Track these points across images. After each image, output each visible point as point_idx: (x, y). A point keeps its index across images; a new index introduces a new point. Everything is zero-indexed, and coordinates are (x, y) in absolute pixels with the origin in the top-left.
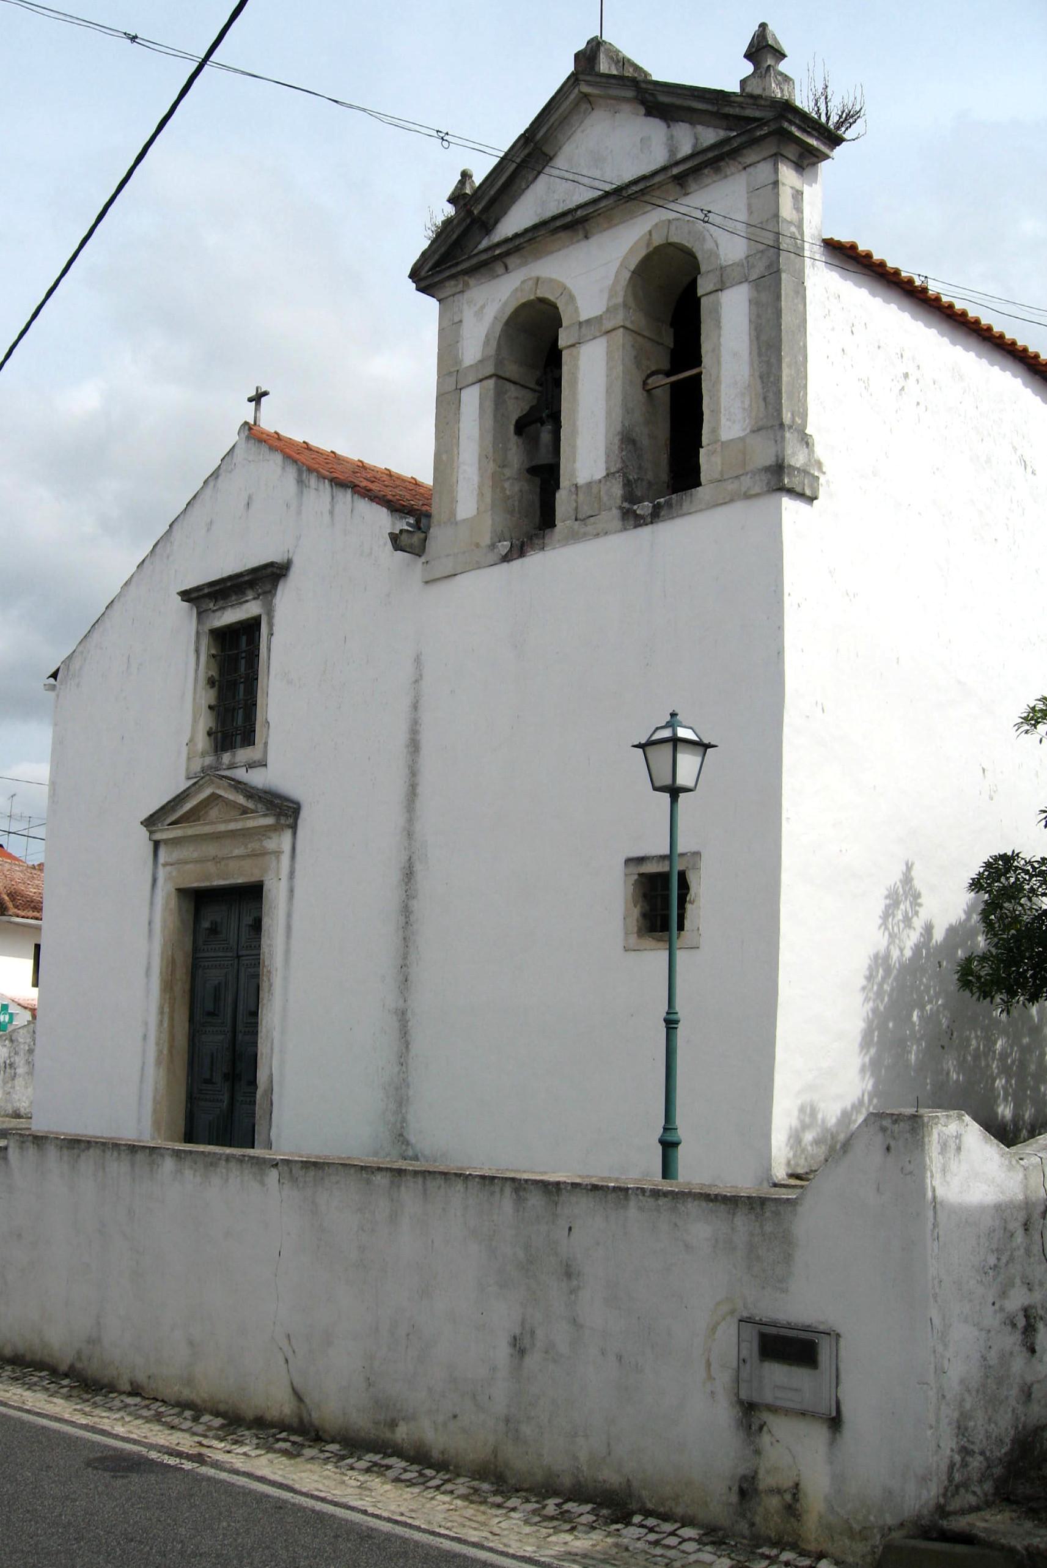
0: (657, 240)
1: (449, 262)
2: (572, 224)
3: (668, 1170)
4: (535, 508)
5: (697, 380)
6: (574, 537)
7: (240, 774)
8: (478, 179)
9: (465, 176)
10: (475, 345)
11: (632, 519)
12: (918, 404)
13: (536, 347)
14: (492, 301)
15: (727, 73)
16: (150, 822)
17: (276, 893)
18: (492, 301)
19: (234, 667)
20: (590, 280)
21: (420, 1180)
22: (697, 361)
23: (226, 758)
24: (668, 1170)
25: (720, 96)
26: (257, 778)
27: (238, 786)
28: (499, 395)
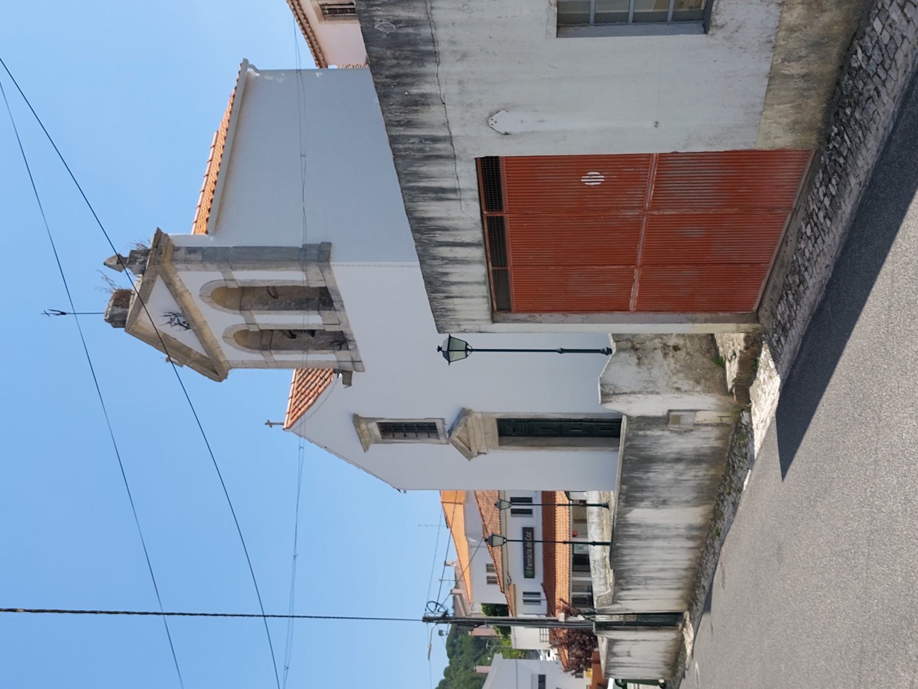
1: (214, 369)
14: (230, 352)
16: (469, 457)
17: (498, 416)
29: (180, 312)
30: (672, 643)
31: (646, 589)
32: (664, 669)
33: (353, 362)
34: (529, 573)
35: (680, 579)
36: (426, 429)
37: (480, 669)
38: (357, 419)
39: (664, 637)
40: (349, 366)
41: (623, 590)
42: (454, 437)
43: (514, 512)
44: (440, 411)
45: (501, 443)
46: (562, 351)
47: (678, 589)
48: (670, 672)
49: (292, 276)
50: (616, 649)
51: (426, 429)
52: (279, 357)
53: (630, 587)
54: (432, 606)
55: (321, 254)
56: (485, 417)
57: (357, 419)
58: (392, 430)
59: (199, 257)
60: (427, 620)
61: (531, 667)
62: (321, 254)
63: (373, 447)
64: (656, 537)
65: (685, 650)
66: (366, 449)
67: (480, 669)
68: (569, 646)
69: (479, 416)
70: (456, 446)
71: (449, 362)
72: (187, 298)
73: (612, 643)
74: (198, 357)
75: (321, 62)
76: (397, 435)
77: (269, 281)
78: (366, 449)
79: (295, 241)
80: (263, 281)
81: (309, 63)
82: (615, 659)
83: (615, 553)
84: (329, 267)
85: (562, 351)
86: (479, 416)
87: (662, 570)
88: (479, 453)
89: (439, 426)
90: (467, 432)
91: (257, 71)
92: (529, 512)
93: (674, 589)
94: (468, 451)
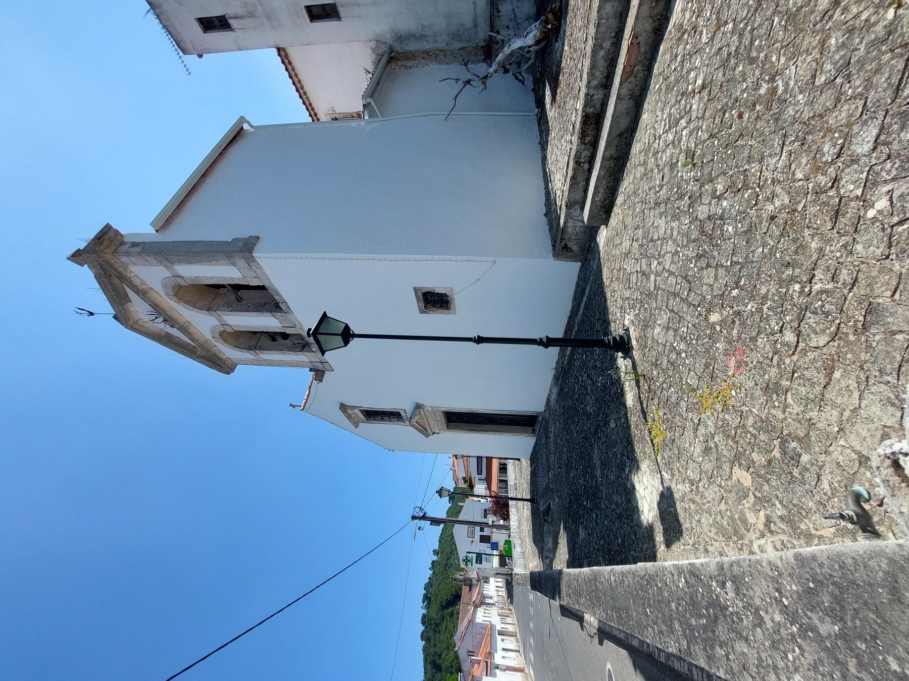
0: (175, 299)
1: (225, 367)
2: (184, 329)
11: (289, 311)
14: (228, 352)
16: (427, 436)
17: (443, 409)
18: (228, 352)
20: (204, 323)
34: (479, 472)
36: (393, 416)
37: (460, 504)
40: (320, 366)
42: (414, 422)
44: (404, 405)
45: (448, 428)
46: (480, 340)
49: (225, 272)
51: (393, 416)
52: (266, 356)
55: (245, 248)
56: (434, 411)
57: (343, 407)
58: (372, 415)
59: (138, 249)
62: (245, 248)
63: (361, 425)
67: (460, 504)
70: (416, 428)
72: (153, 295)
76: (377, 418)
77: (212, 278)
79: (226, 235)
80: (206, 278)
85: (480, 340)
86: (430, 409)
88: (434, 433)
89: (403, 414)
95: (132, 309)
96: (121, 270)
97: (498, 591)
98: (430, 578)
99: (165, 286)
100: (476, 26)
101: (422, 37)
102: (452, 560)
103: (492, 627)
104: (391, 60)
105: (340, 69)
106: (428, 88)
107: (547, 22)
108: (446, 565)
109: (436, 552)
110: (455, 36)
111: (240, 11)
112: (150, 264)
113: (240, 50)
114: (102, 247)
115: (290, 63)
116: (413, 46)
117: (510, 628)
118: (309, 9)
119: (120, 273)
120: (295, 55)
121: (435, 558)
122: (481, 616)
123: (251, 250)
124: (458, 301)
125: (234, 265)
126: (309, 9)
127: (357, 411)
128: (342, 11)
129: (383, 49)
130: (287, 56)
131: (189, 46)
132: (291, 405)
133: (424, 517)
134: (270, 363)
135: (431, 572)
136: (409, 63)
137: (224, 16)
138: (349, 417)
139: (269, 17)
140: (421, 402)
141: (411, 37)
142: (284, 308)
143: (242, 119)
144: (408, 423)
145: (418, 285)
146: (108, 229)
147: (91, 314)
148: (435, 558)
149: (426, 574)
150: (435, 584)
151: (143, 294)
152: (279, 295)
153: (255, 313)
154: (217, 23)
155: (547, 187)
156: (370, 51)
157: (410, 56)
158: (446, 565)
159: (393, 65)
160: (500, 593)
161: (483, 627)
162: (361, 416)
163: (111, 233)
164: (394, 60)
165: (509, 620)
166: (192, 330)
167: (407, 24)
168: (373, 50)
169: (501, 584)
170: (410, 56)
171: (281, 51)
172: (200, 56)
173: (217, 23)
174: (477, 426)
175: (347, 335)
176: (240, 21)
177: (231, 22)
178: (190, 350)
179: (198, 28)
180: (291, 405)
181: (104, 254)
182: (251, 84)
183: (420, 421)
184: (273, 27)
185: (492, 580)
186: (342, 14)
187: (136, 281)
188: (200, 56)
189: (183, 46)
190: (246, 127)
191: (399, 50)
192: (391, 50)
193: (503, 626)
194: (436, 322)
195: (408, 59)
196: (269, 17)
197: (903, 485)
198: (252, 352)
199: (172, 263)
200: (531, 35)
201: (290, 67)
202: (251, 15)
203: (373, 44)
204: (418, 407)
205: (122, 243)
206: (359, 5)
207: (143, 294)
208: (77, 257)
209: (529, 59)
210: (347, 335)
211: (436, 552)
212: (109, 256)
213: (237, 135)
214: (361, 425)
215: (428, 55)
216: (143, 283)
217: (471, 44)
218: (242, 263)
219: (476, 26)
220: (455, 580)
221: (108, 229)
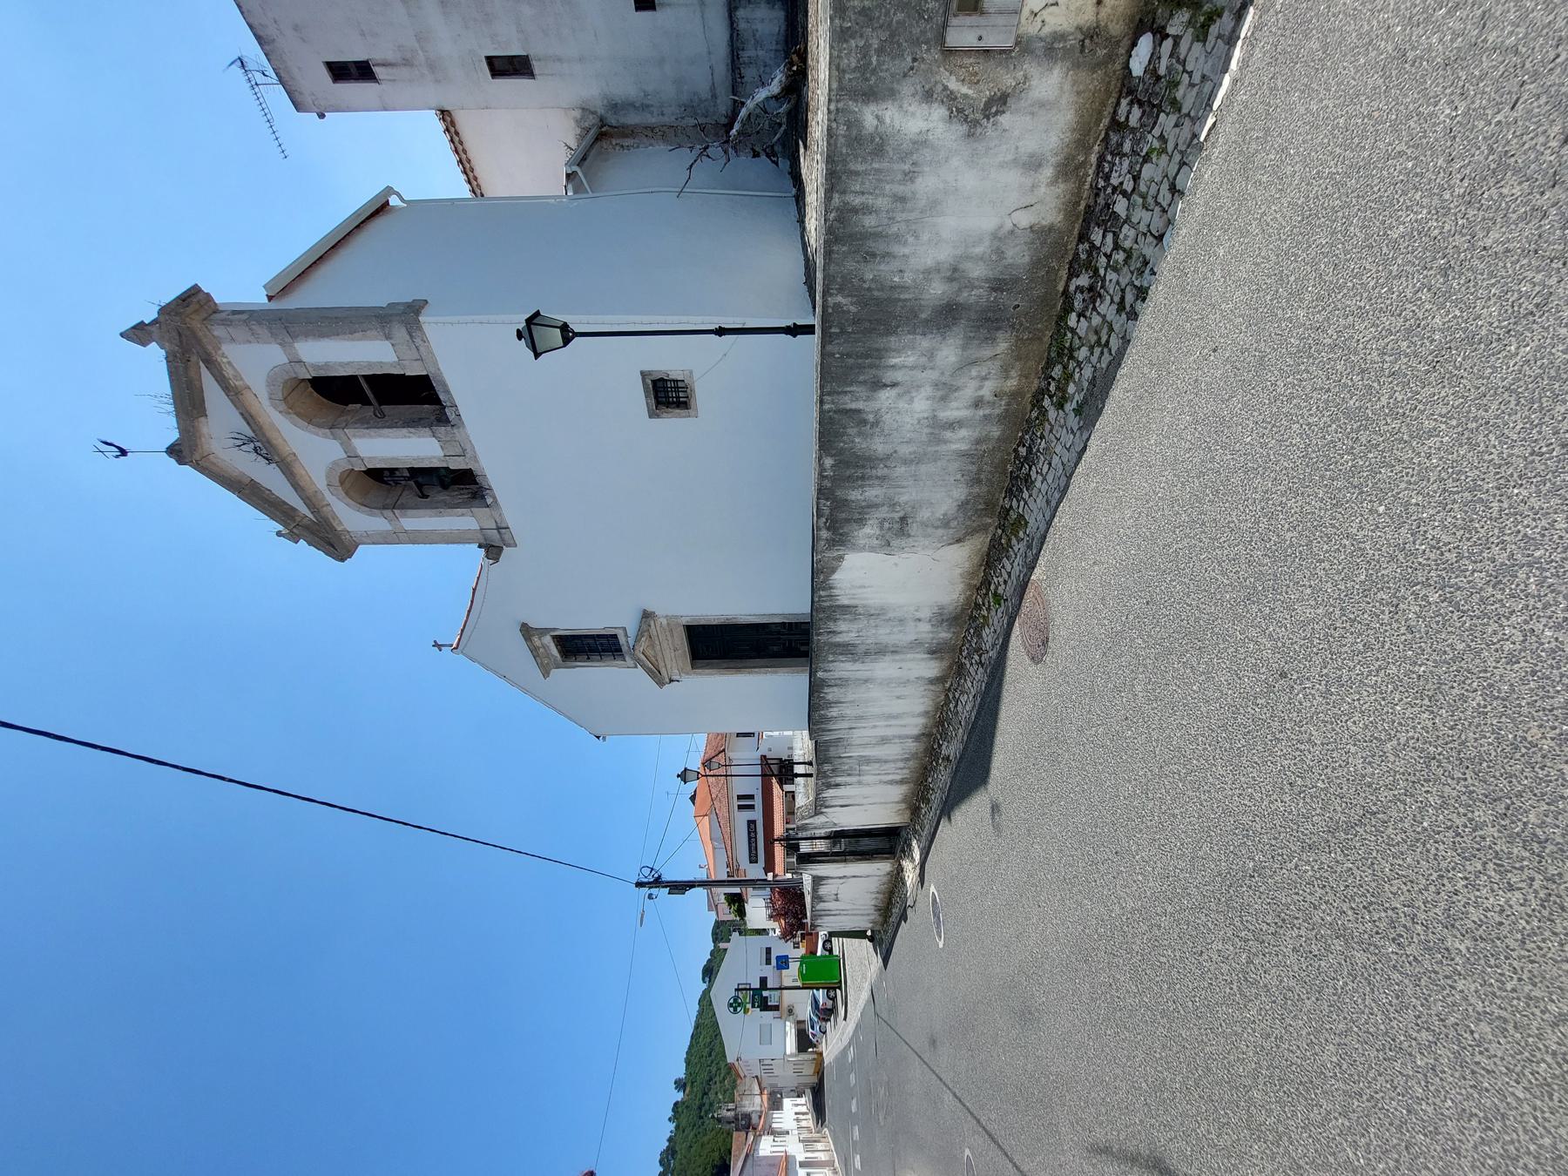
0: (283, 407)
1: (337, 545)
2: (287, 467)
3: (809, 330)
4: (457, 484)
5: (370, 379)
6: (475, 459)
7: (631, 643)
8: (281, 528)
9: (279, 534)
10: (377, 522)
11: (458, 424)
12: (667, 395)
13: (387, 486)
14: (349, 516)
15: (154, 356)
16: (661, 683)
17: (684, 621)
18: (349, 516)
19: (580, 647)
20: (320, 452)
21: (831, 694)
22: (353, 379)
23: (625, 648)
24: (809, 330)
25: (170, 359)
26: (632, 632)
27: (637, 640)
28: (403, 507)
29: (251, 434)
30: (885, 879)
31: (860, 783)
32: (875, 916)
33: (498, 529)
34: (753, 859)
35: (907, 759)
38: (527, 631)
39: (878, 869)
41: (829, 786)
43: (740, 807)
46: (721, 332)
47: (902, 782)
48: (880, 919)
50: (823, 891)
53: (839, 780)
54: (646, 872)
55: (407, 315)
57: (527, 631)
59: (245, 317)
60: (639, 885)
61: (760, 942)
62: (407, 315)
63: (554, 672)
64: (881, 651)
65: (904, 884)
66: (546, 674)
68: (785, 915)
69: (664, 622)
71: (537, 355)
72: (248, 397)
73: (817, 881)
74: (305, 521)
75: (476, 190)
78: (546, 674)
81: (464, 191)
82: (821, 906)
83: (816, 716)
84: (420, 328)
85: (721, 332)
86: (664, 622)
87: (884, 740)
90: (652, 646)
91: (402, 200)
92: (752, 807)
93: (891, 782)
94: (658, 676)
95: (204, 430)
96: (210, 348)
97: (798, 1120)
98: (670, 1140)
99: (271, 382)
100: (714, 96)
101: (645, 107)
102: (712, 1095)
103: (788, 1159)
104: (601, 136)
105: (527, 146)
106: (654, 170)
107: (792, 64)
108: (700, 1108)
109: (680, 1085)
110: (690, 108)
111: (390, 56)
112: (258, 340)
113: (385, 109)
114: (189, 310)
115: (457, 133)
116: (632, 119)
117: (822, 1157)
118: (490, 60)
119: (209, 354)
120: (463, 121)
121: (680, 1096)
122: (766, 1147)
123: (418, 312)
124: (702, 396)
125: (388, 337)
126: (490, 60)
127: (548, 640)
128: (537, 67)
129: (591, 120)
130: (453, 123)
131: (308, 100)
132: (436, 645)
133: (658, 882)
134: (416, 538)
135: (672, 1126)
136: (627, 142)
137: (367, 62)
138: (534, 651)
139: (432, 66)
140: (650, 609)
141: (629, 105)
142: (452, 417)
143: (389, 191)
144: (629, 661)
145: (646, 368)
146: (195, 290)
147: (123, 452)
148: (680, 1096)
149: (662, 1130)
150: (681, 1148)
151: (233, 392)
152: (448, 392)
153: (405, 431)
154: (353, 70)
155: (803, 237)
156: (573, 124)
157: (627, 132)
158: (700, 1108)
159: (604, 144)
160: (804, 1124)
161: (772, 1162)
162: (554, 651)
163: (200, 296)
164: (604, 137)
165: (819, 1146)
166: (297, 470)
167: (625, 89)
168: (577, 122)
169: (804, 1109)
170: (627, 132)
171: (444, 114)
172: (322, 116)
173: (353, 70)
174: (738, 663)
175: (567, 334)
176: (389, 70)
177: (375, 69)
178: (285, 513)
179: (325, 76)
180: (436, 645)
181: (186, 331)
182: (396, 150)
183: (650, 653)
184: (437, 81)
185: (787, 1102)
186: (536, 71)
187: (228, 372)
188: (322, 116)
189: (299, 98)
190: (394, 201)
191: (614, 123)
192: (602, 122)
193: (809, 1155)
194: (669, 358)
195: (625, 136)
196: (432, 66)
197: (1009, 226)
198: (388, 513)
199: (294, 337)
200: (776, 81)
201: (456, 139)
202: (407, 63)
203: (577, 114)
204: (647, 616)
205: (216, 311)
206: (560, 60)
207: (233, 392)
208: (139, 333)
209: (780, 125)
210: (567, 334)
211: (680, 1085)
212: (196, 323)
213: (380, 209)
214: (554, 672)
215: (652, 133)
216: (238, 376)
217: (708, 120)
218: (400, 333)
219: (714, 96)
220: (719, 1120)
221: (195, 290)
